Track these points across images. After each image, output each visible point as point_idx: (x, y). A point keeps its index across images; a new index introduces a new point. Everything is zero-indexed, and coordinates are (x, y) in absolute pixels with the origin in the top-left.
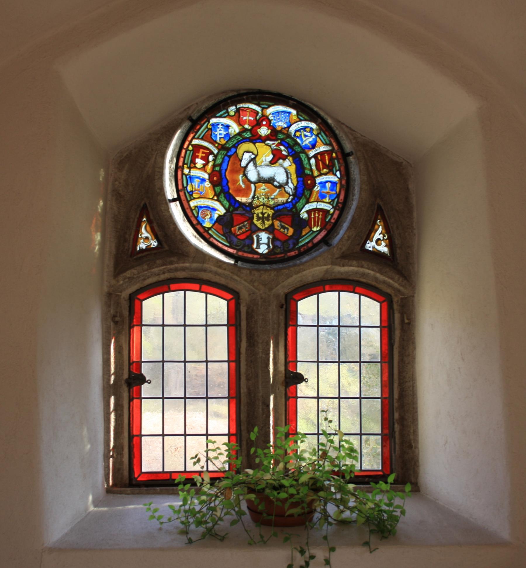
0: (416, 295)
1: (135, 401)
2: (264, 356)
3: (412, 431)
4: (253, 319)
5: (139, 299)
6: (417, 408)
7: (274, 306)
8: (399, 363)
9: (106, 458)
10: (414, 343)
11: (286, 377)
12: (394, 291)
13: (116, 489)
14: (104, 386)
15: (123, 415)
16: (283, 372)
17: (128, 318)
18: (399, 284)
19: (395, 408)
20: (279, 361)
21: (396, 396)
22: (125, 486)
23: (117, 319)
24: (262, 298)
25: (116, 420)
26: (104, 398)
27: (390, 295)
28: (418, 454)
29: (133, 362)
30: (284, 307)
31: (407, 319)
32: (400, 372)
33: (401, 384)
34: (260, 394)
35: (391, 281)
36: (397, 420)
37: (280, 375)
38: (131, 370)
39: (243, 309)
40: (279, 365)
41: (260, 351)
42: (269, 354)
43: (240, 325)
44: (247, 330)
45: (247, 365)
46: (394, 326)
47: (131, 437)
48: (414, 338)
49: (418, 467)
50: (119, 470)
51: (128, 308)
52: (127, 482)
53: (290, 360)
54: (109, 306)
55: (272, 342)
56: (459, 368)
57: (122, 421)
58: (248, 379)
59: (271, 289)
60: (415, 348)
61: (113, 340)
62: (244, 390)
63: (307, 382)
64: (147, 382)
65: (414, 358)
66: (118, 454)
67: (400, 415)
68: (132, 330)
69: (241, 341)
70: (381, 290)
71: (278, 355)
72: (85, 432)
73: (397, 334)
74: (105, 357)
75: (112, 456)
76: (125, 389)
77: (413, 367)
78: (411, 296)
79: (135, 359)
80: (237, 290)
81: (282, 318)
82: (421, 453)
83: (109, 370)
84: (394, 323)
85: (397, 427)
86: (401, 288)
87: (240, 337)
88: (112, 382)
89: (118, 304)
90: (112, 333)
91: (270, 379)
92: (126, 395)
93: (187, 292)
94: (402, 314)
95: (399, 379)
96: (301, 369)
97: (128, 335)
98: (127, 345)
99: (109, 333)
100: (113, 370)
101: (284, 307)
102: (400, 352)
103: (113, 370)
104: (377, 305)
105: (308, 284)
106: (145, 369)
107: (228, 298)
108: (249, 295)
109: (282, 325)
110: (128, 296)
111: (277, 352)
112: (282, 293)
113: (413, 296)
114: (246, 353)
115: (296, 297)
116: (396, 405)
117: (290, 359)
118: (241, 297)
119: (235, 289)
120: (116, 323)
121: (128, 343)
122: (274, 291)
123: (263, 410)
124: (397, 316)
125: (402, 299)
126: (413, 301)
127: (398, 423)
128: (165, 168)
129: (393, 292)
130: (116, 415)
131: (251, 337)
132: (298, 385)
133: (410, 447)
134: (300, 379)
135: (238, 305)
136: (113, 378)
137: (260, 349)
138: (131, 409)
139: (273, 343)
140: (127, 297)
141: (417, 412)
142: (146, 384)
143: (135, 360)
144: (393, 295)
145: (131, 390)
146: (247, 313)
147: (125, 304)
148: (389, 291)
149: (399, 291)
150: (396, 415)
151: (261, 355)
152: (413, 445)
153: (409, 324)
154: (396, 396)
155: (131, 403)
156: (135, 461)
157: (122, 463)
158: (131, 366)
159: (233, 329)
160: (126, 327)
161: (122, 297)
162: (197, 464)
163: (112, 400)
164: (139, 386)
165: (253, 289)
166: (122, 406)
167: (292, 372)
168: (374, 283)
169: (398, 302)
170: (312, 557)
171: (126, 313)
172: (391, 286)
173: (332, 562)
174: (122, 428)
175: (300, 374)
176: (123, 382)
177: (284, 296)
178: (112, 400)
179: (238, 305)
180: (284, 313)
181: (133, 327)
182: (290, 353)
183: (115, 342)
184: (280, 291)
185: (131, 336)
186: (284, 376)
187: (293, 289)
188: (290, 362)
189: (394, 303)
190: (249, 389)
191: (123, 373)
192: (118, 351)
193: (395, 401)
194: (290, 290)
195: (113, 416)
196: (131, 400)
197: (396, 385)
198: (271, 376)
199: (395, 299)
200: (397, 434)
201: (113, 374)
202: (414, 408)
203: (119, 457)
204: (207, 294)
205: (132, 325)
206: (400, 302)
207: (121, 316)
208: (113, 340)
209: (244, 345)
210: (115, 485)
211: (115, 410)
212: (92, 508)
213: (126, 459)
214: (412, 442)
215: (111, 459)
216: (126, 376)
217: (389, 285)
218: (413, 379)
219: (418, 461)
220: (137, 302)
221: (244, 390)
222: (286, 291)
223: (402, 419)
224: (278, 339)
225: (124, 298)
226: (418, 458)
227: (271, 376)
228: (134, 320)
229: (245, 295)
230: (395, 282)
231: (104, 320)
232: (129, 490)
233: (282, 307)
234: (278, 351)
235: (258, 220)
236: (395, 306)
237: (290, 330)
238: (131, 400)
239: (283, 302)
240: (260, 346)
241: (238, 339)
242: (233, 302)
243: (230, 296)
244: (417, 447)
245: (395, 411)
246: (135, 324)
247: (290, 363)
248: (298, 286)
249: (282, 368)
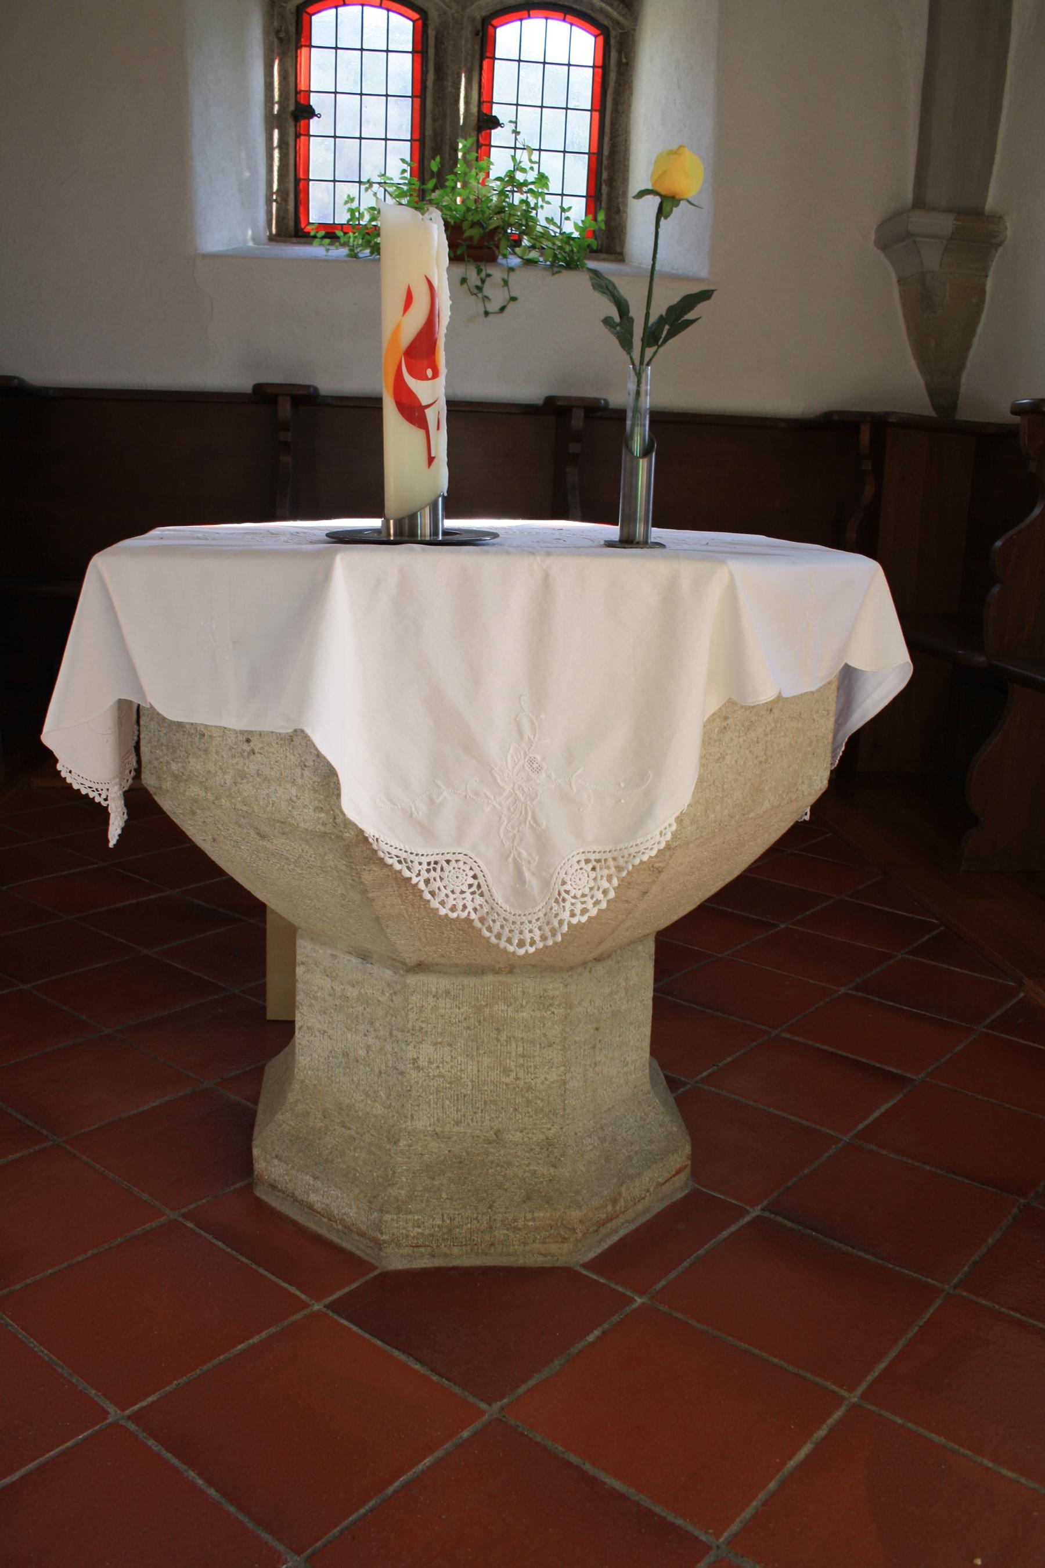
0: (637, 28)
1: (302, 138)
2: (453, 90)
3: (621, 193)
4: (443, 46)
5: (308, 14)
6: (628, 166)
7: (467, 32)
8: (612, 113)
9: (269, 201)
10: (631, 88)
11: (479, 120)
12: (612, 23)
13: (278, 238)
14: (266, 114)
15: (288, 155)
16: (476, 114)
17: (294, 36)
18: (618, 13)
19: (603, 166)
20: (472, 101)
21: (606, 152)
22: (290, 237)
23: (282, 35)
24: (453, 19)
25: (281, 160)
26: (266, 130)
27: (608, 28)
28: (626, 219)
29: (301, 91)
30: (481, 34)
31: (626, 58)
32: (613, 124)
33: (614, 137)
34: (448, 137)
35: (609, 8)
36: (605, 181)
37: (472, 118)
38: (298, 100)
39: (432, 33)
40: (472, 106)
41: (449, 84)
42: (459, 89)
43: (427, 52)
44: (435, 59)
45: (434, 102)
46: (609, 66)
47: (297, 181)
48: (632, 81)
49: (625, 234)
50: (283, 218)
51: (295, 24)
52: (293, 232)
53: (485, 100)
54: (272, 17)
55: (463, 75)
56: (675, 100)
57: (288, 161)
58: (434, 120)
59: (464, 8)
60: (631, 94)
61: (277, 63)
62: (429, 132)
63: (502, 127)
64: (316, 116)
65: (629, 106)
66: (282, 200)
67: (609, 175)
68: (299, 51)
69: (427, 72)
70: (597, 21)
71: (471, 94)
72: (243, 155)
73: (612, 77)
74: (268, 80)
75: (276, 201)
76: (291, 122)
77: (628, 117)
78: (632, 29)
79: (303, 87)
80: (425, 8)
81: (477, 48)
82: (629, 219)
83: (272, 97)
84: (609, 63)
85: (604, 189)
86: (621, 19)
87: (427, 67)
88: (276, 112)
89: (283, 18)
90: (276, 51)
91: (459, 119)
92: (291, 131)
93: (365, 8)
94: (620, 53)
95: (611, 133)
96: (497, 111)
97: (294, 56)
98: (294, 70)
99: (272, 51)
100: (276, 98)
101: (481, 34)
102: (614, 100)
103: (276, 98)
104: (591, 39)
105: (509, 7)
106: (315, 101)
107: (414, 19)
108: (440, 16)
109: (477, 57)
110: (295, 8)
111: (469, 90)
112: (479, 17)
113: (634, 30)
114: (433, 89)
115: (495, 22)
116: (605, 163)
117: (484, 98)
118: (430, 18)
119: (422, 6)
120: (281, 40)
121: (294, 66)
122: (468, 10)
123: (450, 155)
124: (614, 54)
125: (621, 34)
126: (633, 35)
127: (606, 185)
128: (340, 527)
129: (611, 24)
130: (280, 153)
131: (440, 69)
132: (493, 131)
133: (618, 211)
134: (495, 123)
135: (425, 26)
136: (276, 107)
137: (449, 83)
138: (298, 148)
139: (465, 77)
140: (293, 9)
141: (628, 171)
142: (316, 118)
143: (303, 89)
144: (610, 28)
145: (298, 124)
146: (436, 38)
147: (291, 19)
148: (606, 22)
149: (618, 23)
150: (605, 175)
151: (450, 89)
152: (621, 208)
153: (627, 64)
154: (606, 152)
155: (298, 140)
156: (301, 209)
157: (287, 210)
158: (298, 96)
159: (418, 57)
160: (293, 47)
161: (288, 8)
162: (369, 190)
163: (276, 133)
164: (307, 121)
165: (444, 6)
166: (287, 144)
167: (486, 115)
168: (589, 12)
169: (616, 37)
170: (488, 276)
171: (292, 30)
172: (609, 17)
173: (511, 282)
174: (287, 170)
175: (495, 117)
176: (289, 115)
177: (480, 21)
178: (276, 133)
179: (425, 26)
180: (479, 41)
181: (301, 46)
182: (484, 91)
183: (280, 64)
184: (477, 14)
185: (299, 59)
186: (476, 119)
187: (491, 12)
188: (484, 102)
189: (611, 38)
190: (435, 132)
191: (288, 104)
192: (283, 77)
193: (604, 158)
194: (488, 13)
195: (276, 154)
196: (297, 136)
197: (607, 139)
198: (462, 117)
199: (613, 34)
200: (604, 197)
201: (277, 103)
202: (625, 166)
203: (283, 203)
204: (388, 10)
205: (299, 45)
206: (618, 38)
207: (287, 32)
208: (277, 63)
209: (431, 77)
210: (278, 234)
211: (280, 146)
212: (251, 244)
213: (291, 207)
214: (621, 205)
215: (274, 204)
216: (292, 108)
217: (608, 16)
218: (627, 132)
219: (625, 228)
220: (305, 16)
221: (429, 132)
222: (484, 13)
223: (611, 181)
224: (472, 75)
225: (290, 10)
226: (625, 225)
227: (462, 117)
228: (302, 39)
229: (433, 15)
230: (614, 10)
231: (266, 33)
232: (294, 240)
233: (477, 34)
234: (471, 89)
235: (647, 1146)
236: (613, 42)
237: (486, 63)
238: (297, 136)
239: (479, 27)
240: (450, 78)
241: (424, 69)
242: (420, 23)
243: (416, 16)
244: (625, 212)
245: (603, 170)
246: (303, 44)
247: (485, 104)
248: (499, 8)
249: (474, 110)
